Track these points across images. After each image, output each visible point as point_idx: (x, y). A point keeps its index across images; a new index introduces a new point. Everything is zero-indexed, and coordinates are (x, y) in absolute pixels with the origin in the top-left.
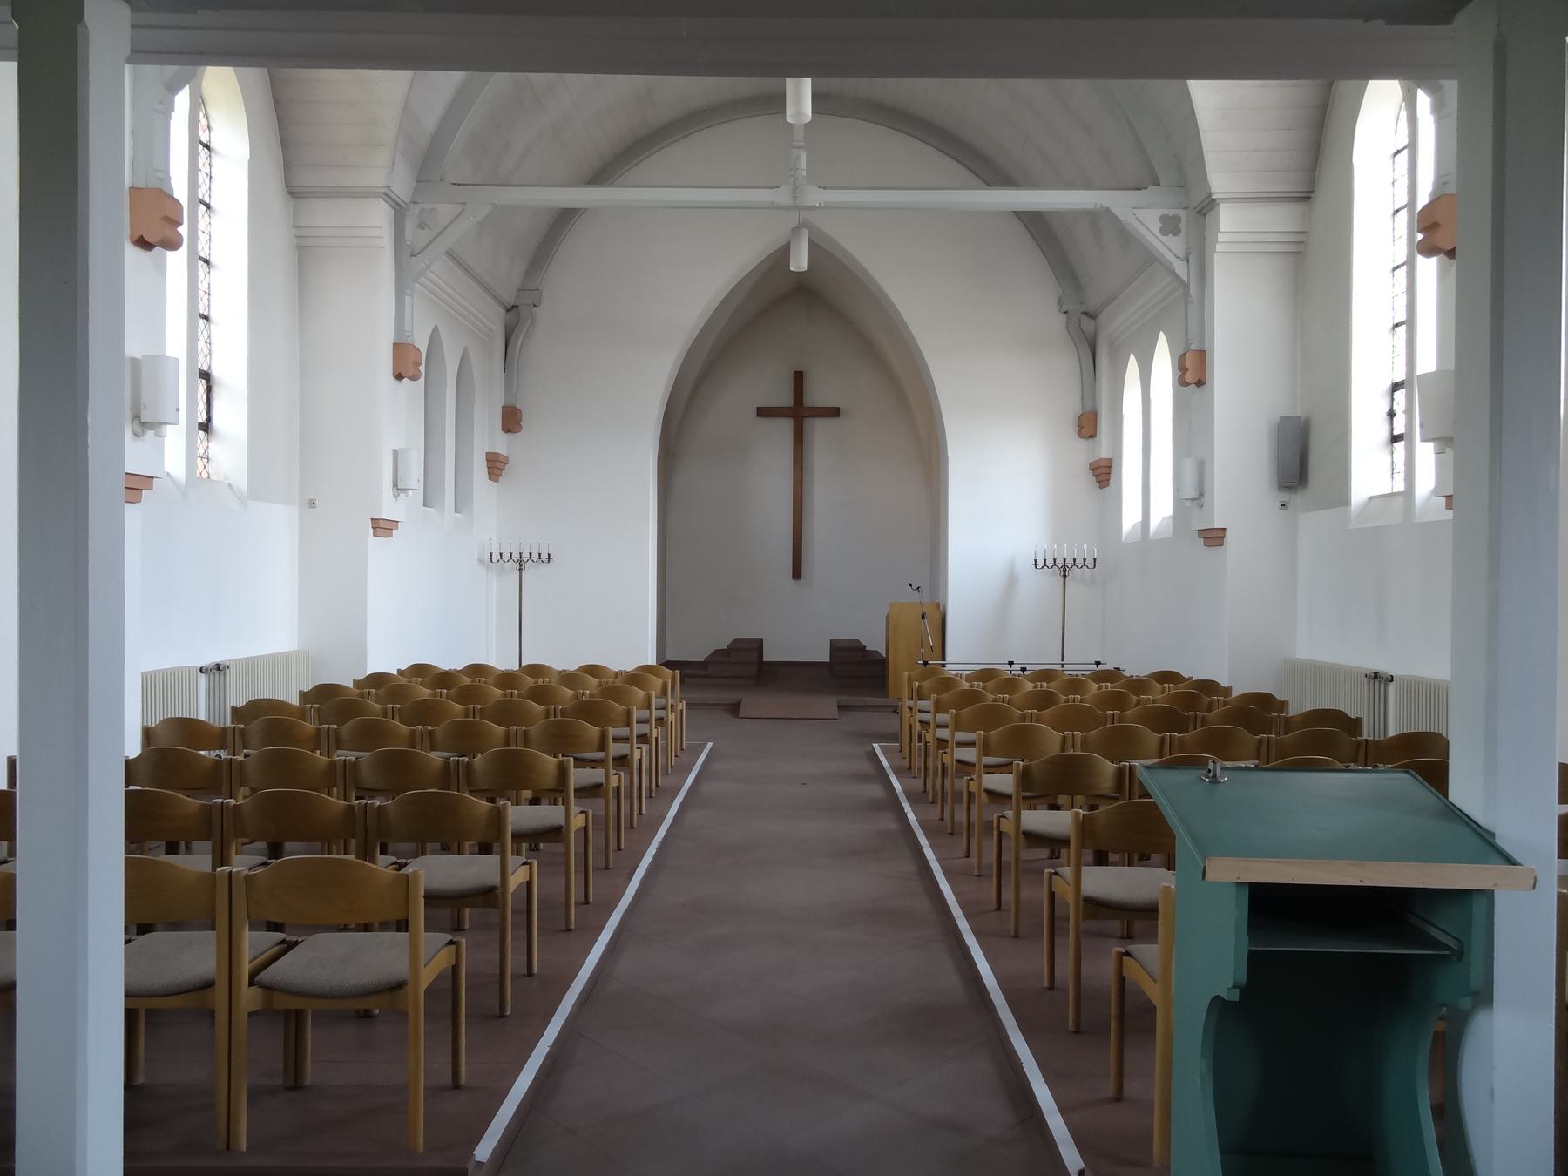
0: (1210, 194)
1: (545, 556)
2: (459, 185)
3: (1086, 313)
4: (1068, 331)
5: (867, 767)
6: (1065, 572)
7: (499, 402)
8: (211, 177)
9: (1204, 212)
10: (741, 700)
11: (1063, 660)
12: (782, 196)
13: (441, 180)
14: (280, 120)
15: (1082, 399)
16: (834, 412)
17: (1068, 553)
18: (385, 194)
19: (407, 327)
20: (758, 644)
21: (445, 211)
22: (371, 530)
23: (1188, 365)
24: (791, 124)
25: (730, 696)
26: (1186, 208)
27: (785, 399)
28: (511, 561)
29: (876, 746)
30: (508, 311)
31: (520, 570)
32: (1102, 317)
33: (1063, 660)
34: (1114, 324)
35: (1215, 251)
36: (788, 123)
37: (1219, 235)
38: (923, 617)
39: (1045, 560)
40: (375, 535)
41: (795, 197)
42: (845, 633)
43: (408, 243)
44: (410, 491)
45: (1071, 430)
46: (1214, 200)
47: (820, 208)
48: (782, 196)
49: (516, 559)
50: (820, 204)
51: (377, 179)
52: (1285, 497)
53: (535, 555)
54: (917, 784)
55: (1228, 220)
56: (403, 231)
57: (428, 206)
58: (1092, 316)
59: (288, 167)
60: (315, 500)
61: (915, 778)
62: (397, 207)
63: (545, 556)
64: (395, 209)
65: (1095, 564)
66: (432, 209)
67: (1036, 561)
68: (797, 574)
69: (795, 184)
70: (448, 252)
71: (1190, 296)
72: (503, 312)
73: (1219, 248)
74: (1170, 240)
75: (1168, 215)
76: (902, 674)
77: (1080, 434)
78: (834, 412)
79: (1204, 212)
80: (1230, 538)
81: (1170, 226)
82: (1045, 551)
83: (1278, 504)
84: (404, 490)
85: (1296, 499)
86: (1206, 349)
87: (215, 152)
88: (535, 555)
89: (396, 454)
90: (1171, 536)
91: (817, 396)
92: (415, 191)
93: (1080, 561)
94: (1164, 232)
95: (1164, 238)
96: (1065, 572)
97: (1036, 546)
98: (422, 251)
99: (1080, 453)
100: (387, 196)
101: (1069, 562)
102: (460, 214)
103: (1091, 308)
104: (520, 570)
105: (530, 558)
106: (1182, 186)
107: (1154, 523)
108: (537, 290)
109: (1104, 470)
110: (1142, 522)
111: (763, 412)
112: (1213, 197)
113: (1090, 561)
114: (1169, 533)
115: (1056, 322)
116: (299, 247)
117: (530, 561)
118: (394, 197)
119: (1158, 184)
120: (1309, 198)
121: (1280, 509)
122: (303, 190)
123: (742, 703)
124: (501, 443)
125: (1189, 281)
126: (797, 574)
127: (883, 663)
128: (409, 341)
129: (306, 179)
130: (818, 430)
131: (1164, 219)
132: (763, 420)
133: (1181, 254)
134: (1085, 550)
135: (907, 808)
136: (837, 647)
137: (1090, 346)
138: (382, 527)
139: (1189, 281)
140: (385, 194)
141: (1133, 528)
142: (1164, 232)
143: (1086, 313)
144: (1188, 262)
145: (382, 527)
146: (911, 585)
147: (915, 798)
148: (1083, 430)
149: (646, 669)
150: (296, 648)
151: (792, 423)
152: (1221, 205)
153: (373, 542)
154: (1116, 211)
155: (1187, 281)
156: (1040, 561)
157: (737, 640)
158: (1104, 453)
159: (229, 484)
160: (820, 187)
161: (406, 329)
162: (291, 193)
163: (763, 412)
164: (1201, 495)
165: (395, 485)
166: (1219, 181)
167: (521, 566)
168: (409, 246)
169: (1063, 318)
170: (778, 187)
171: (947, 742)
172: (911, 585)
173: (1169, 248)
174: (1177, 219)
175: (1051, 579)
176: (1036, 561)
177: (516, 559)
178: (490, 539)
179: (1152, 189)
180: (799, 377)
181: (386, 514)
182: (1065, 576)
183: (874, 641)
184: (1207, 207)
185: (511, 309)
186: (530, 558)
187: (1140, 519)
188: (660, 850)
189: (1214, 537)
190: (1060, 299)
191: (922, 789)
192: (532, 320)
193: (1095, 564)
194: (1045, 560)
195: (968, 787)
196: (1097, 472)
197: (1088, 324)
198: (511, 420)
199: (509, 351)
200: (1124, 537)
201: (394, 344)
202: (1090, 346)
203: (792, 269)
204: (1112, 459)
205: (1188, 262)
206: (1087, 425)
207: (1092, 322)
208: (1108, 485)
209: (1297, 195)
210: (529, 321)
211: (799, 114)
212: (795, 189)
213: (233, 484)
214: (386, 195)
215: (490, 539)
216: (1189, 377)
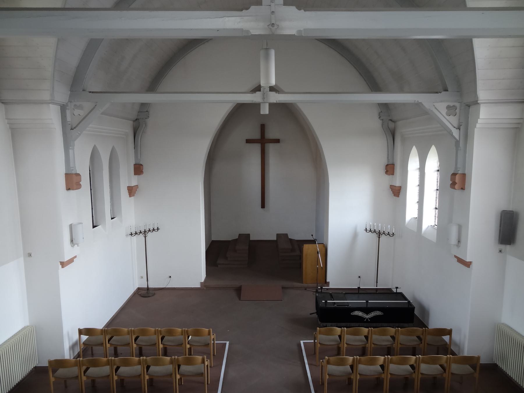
4: (382, 127)
6: (379, 236)
10: (241, 286)
15: (388, 158)
16: (277, 141)
17: (379, 227)
19: (72, 165)
20: (248, 236)
22: (61, 266)
23: (457, 181)
27: (258, 136)
29: (302, 342)
34: (402, 130)
35: (475, 127)
37: (479, 120)
39: (370, 229)
52: (502, 247)
56: (65, 116)
67: (366, 229)
68: (263, 206)
69: (263, 91)
72: (131, 122)
73: (478, 126)
78: (277, 141)
80: (473, 266)
83: (498, 251)
85: (508, 248)
86: (466, 172)
89: (71, 226)
91: (271, 134)
92: (70, 96)
95: (447, 117)
96: (379, 236)
97: (367, 222)
99: (386, 180)
102: (94, 108)
107: (424, 227)
108: (147, 111)
111: (248, 141)
113: (391, 233)
121: (499, 253)
123: (250, 91)
124: (134, 181)
126: (263, 206)
130: (271, 148)
131: (448, 107)
132: (248, 144)
133: (456, 126)
134: (388, 228)
143: (391, 120)
150: (27, 324)
151: (259, 139)
152: (481, 105)
158: (398, 184)
161: (71, 166)
163: (248, 141)
165: (72, 241)
166: (482, 95)
174: (454, 107)
176: (366, 229)
178: (131, 226)
187: (416, 216)
192: (145, 125)
194: (370, 229)
197: (392, 125)
198: (138, 169)
200: (406, 224)
201: (66, 174)
204: (401, 186)
205: (459, 129)
206: (390, 169)
207: (393, 123)
210: (144, 125)
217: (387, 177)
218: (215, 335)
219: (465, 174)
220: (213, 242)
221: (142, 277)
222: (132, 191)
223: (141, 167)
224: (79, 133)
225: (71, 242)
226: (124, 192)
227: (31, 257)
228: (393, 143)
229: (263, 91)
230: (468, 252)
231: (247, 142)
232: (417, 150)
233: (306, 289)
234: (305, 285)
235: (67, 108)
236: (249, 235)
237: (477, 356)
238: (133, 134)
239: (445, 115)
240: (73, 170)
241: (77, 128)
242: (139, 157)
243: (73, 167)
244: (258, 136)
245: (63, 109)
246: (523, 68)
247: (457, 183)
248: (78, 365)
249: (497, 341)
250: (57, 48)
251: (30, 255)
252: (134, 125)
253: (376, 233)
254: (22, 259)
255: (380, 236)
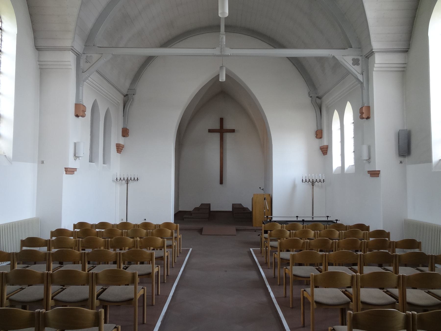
0: (372, 49)
1: (136, 179)
2: (100, 47)
3: (318, 97)
4: (312, 103)
5: (248, 260)
6: (313, 184)
7: (121, 127)
8: (2, 40)
9: (368, 57)
10: (203, 228)
11: (313, 216)
12: (217, 51)
13: (93, 46)
14: (32, 22)
16: (233, 131)
17: (314, 177)
18: (72, 49)
21: (95, 56)
22: (65, 172)
23: (364, 111)
24: (221, 17)
25: (200, 226)
26: (361, 56)
27: (218, 127)
28: (124, 181)
29: (251, 249)
30: (125, 96)
31: (127, 184)
32: (324, 98)
33: (313, 216)
34: (327, 101)
36: (219, 16)
37: (375, 64)
38: (265, 199)
39: (306, 180)
40: (66, 174)
41: (221, 52)
42: (237, 202)
43: (81, 68)
44: (80, 158)
45: (314, 136)
46: (373, 52)
47: (231, 56)
48: (217, 51)
49: (126, 180)
50: (230, 54)
51: (68, 43)
52: (402, 159)
53: (133, 178)
54: (264, 260)
55: (378, 59)
57: (89, 55)
58: (319, 98)
59: (35, 39)
60: (44, 161)
61: (269, 268)
62: (78, 55)
63: (136, 179)
64: (76, 55)
65: (324, 181)
66: (91, 56)
67: (303, 180)
68: (221, 182)
69: (221, 47)
70: (96, 71)
71: (364, 87)
72: (123, 97)
73: (375, 69)
74: (356, 67)
75: (355, 58)
76: (257, 216)
77: (316, 137)
78: (233, 131)
79: (368, 57)
81: (356, 62)
82: (306, 176)
83: (399, 162)
84: (78, 157)
85: (406, 160)
87: (4, 31)
88: (133, 178)
89: (75, 144)
90: (354, 172)
91: (228, 125)
93: (318, 180)
94: (354, 64)
95: (353, 66)
96: (313, 184)
98: (86, 71)
99: (317, 144)
100: (73, 50)
101: (315, 180)
102: (101, 58)
103: (320, 95)
104: (127, 184)
105: (131, 179)
106: (360, 48)
109: (325, 149)
110: (341, 167)
111: (210, 131)
112: (373, 50)
114: (353, 171)
115: (308, 100)
116: (41, 69)
117: (131, 180)
118: (76, 51)
119: (352, 47)
120: (408, 51)
121: (400, 164)
122: (43, 47)
124: (122, 141)
125: (363, 81)
126: (221, 182)
127: (251, 213)
128: (81, 103)
129: (42, 43)
130: (228, 137)
131: (353, 60)
132: (210, 134)
133: (360, 72)
134: (320, 176)
135: (260, 267)
136: (234, 206)
137: (320, 108)
138: (70, 171)
139: (363, 81)
140: (72, 49)
141: (336, 169)
142: (354, 64)
143: (318, 97)
144: (363, 75)
145: (70, 171)
146: (260, 188)
147: (273, 281)
148: (318, 136)
149: (167, 225)
151: (219, 129)
152: (375, 54)
153: (66, 178)
154: (337, 57)
155: (362, 81)
156: (304, 180)
157: (202, 204)
158: (325, 144)
159: (5, 156)
160: (230, 48)
162: (37, 49)
163: (210, 131)
164: (370, 158)
165: (75, 155)
166: (376, 45)
167: (127, 182)
168: (82, 69)
169: (310, 98)
170: (215, 48)
171: (277, 248)
172: (260, 188)
173: (356, 70)
174: (358, 60)
175: (308, 186)
176: (303, 180)
177: (126, 180)
178: (117, 173)
179: (349, 49)
180: (222, 120)
181: (71, 166)
182: (313, 185)
183: (248, 204)
184: (372, 53)
185: (126, 96)
186: (131, 179)
187: (340, 166)
188: (163, 322)
189: (375, 174)
190: (309, 92)
191: (284, 295)
192: (133, 99)
193: (324, 181)
194: (306, 180)
195: (303, 295)
196: (323, 150)
197: (318, 101)
198: (125, 133)
199: (124, 111)
201: (75, 104)
202: (320, 108)
203: (220, 80)
206: (319, 134)
208: (327, 154)
209: (401, 50)
210: (132, 100)
211: (223, 13)
212: (221, 49)
213: (7, 155)
214: (73, 50)
215: (117, 173)
216: (364, 116)
217: (317, 140)
218: (181, 235)
219: (370, 106)
220: (180, 212)
221: (122, 220)
222: (119, 148)
223: (128, 130)
224: (88, 75)
225: (74, 156)
226: (113, 149)
227: (44, 164)
228: (320, 116)
229: (221, 47)
230: (376, 159)
231: (209, 132)
232: (338, 113)
233: (255, 231)
234: (254, 228)
235: (81, 57)
236: (209, 205)
237: (388, 232)
238: (123, 105)
239: (351, 65)
240: (81, 101)
241: (87, 72)
242: (126, 123)
243: (81, 100)
244: (218, 127)
245: (78, 56)
246: (401, 26)
247: (364, 113)
248: (74, 235)
249: (405, 229)
250: (80, 9)
251: (43, 162)
252: (124, 99)
253: (310, 182)
254: (36, 165)
255: (314, 184)
